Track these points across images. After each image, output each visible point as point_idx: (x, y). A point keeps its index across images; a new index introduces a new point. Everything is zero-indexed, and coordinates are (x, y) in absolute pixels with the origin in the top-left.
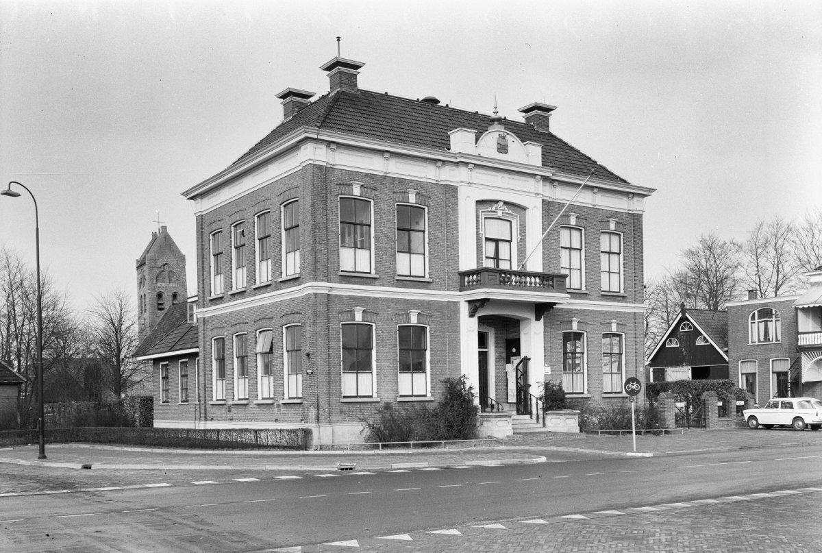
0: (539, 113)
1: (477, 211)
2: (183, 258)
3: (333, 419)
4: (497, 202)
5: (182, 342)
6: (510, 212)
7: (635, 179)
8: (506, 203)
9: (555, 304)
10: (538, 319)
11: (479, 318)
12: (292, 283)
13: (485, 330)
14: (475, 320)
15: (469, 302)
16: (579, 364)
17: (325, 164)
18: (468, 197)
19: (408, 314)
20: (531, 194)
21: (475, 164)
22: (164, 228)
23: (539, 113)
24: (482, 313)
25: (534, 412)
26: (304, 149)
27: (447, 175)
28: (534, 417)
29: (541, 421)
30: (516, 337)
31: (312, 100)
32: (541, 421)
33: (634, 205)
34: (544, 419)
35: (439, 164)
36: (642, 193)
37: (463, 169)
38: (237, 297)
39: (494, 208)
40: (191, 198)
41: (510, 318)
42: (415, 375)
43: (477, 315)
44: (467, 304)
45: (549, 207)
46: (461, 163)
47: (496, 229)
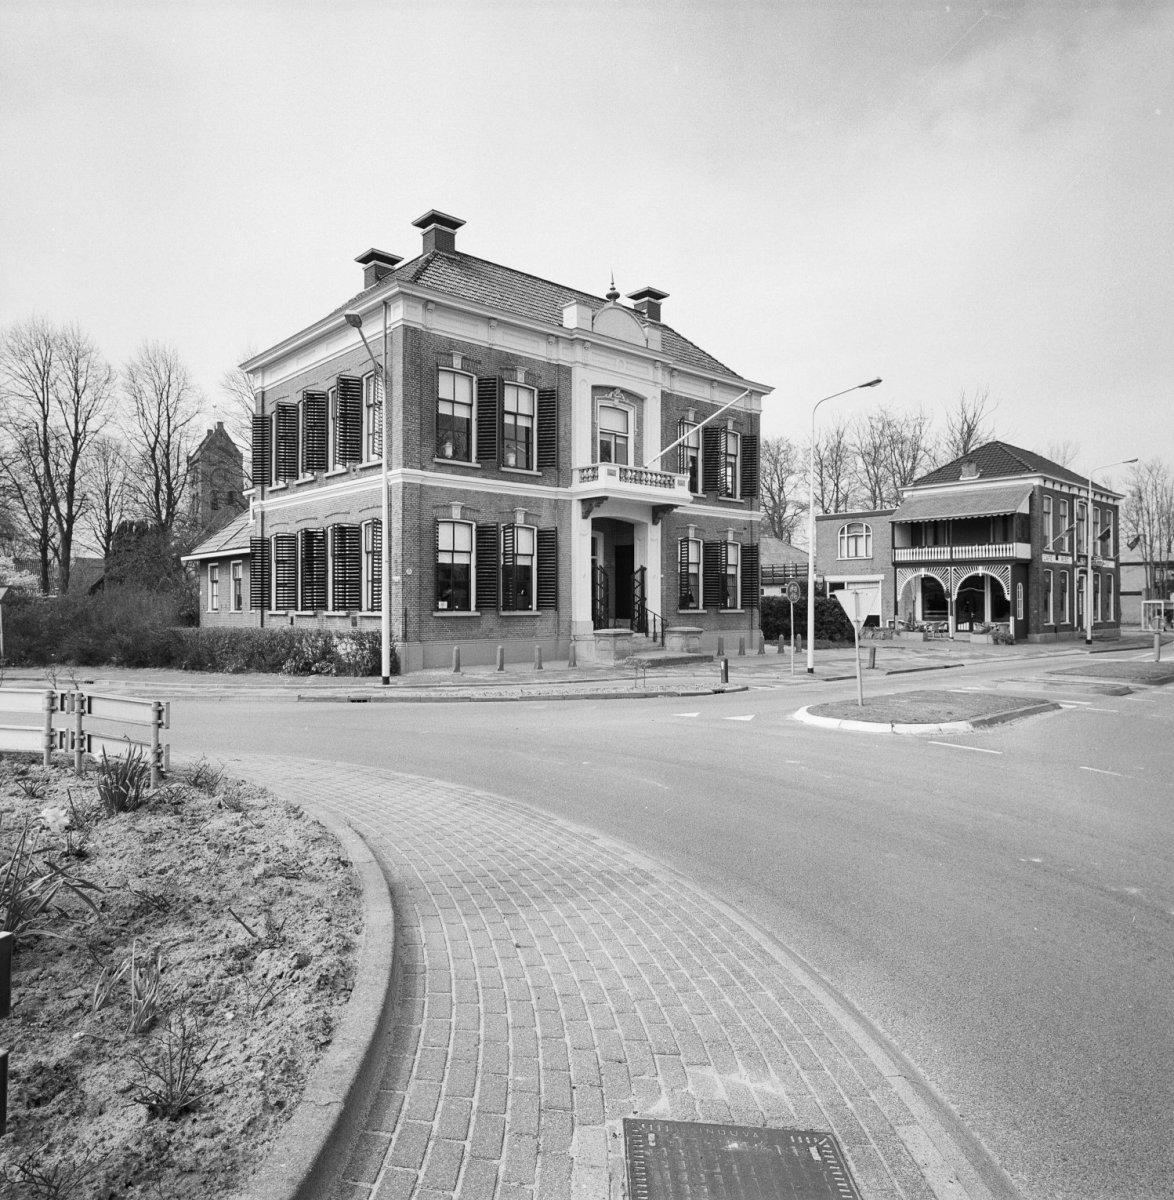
0: (650, 301)
1: (593, 398)
2: (241, 456)
3: (424, 636)
4: (613, 389)
5: (234, 541)
6: (627, 401)
7: (749, 372)
8: (623, 391)
9: (676, 506)
10: (655, 523)
11: (593, 520)
12: (307, 487)
13: (595, 536)
14: (588, 523)
15: (583, 501)
16: (487, 539)
17: (421, 327)
18: (584, 380)
19: (513, 512)
20: (650, 384)
21: (592, 343)
22: (220, 424)
23: (650, 301)
24: (598, 513)
25: (651, 628)
26: (395, 308)
27: (561, 355)
28: (651, 635)
29: (659, 640)
30: (629, 543)
31: (397, 266)
32: (659, 640)
33: (752, 405)
34: (663, 637)
35: (552, 339)
36: (759, 391)
37: (578, 349)
38: (368, 472)
39: (611, 395)
40: (251, 372)
41: (621, 522)
42: (450, 562)
43: (593, 515)
44: (580, 504)
45: (666, 397)
46: (572, 340)
47: (611, 422)
